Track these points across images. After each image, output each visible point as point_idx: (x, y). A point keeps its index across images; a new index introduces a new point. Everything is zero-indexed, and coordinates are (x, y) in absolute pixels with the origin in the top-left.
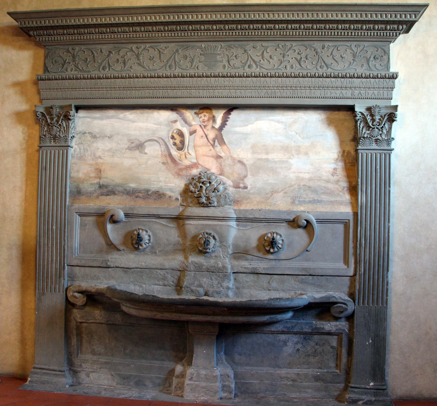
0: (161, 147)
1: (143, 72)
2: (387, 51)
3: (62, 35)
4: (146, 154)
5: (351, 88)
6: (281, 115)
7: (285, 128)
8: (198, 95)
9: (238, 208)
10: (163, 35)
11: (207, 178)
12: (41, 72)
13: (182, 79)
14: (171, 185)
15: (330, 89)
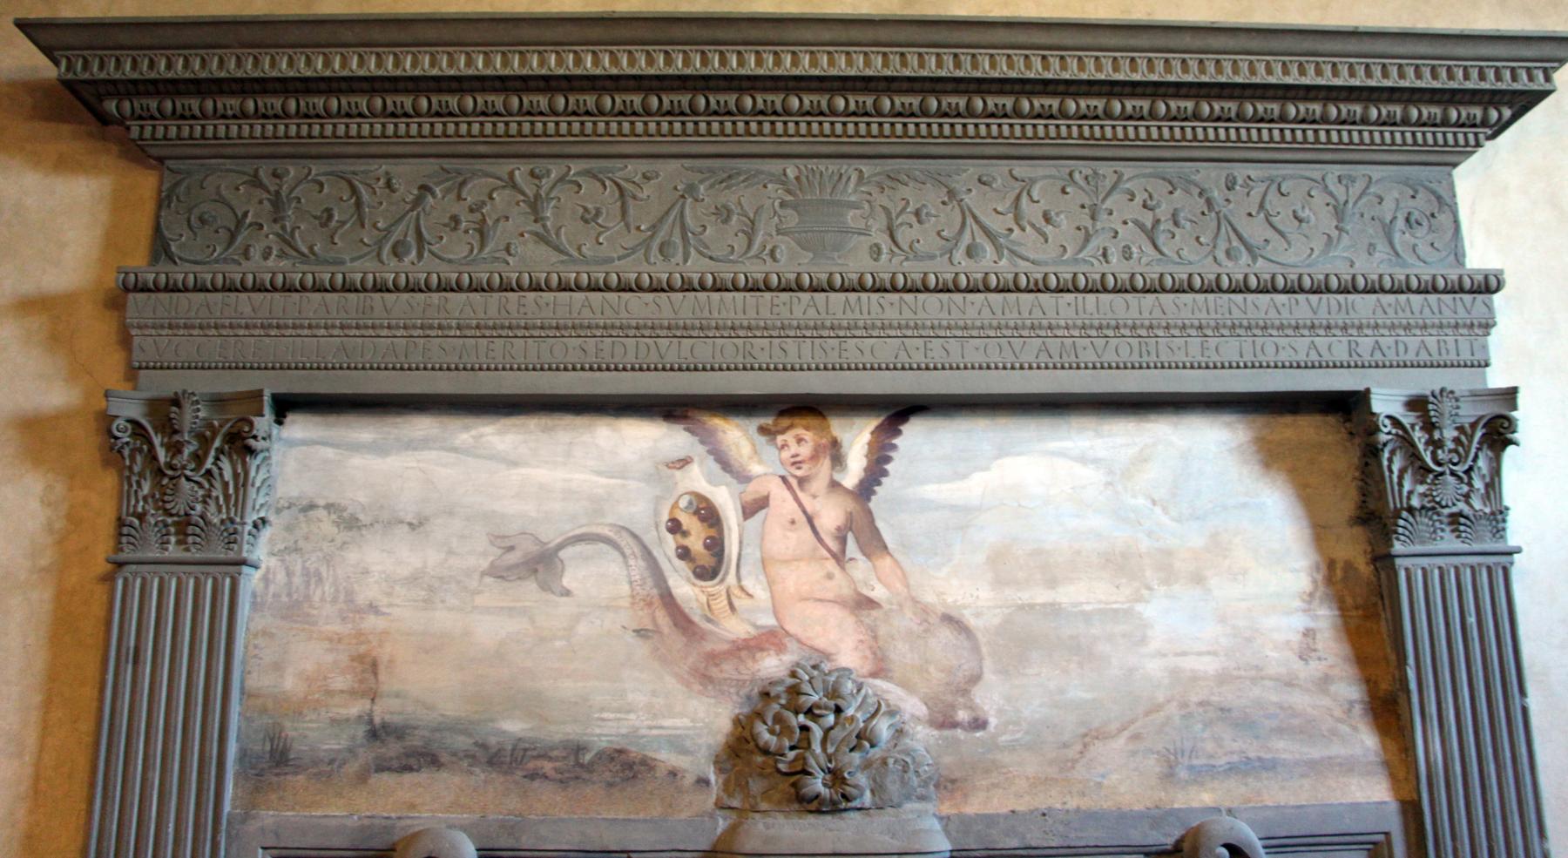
0: (628, 566)
1: (561, 268)
2: (1448, 201)
3: (235, 117)
4: (567, 593)
5: (1345, 328)
6: (1091, 433)
7: (1109, 484)
8: (778, 357)
9: (954, 811)
10: (640, 127)
11: (825, 689)
12: (138, 260)
13: (716, 296)
14: (676, 724)
15: (1274, 332)
